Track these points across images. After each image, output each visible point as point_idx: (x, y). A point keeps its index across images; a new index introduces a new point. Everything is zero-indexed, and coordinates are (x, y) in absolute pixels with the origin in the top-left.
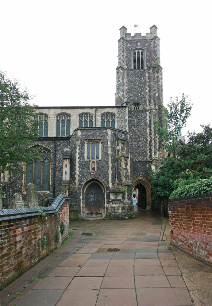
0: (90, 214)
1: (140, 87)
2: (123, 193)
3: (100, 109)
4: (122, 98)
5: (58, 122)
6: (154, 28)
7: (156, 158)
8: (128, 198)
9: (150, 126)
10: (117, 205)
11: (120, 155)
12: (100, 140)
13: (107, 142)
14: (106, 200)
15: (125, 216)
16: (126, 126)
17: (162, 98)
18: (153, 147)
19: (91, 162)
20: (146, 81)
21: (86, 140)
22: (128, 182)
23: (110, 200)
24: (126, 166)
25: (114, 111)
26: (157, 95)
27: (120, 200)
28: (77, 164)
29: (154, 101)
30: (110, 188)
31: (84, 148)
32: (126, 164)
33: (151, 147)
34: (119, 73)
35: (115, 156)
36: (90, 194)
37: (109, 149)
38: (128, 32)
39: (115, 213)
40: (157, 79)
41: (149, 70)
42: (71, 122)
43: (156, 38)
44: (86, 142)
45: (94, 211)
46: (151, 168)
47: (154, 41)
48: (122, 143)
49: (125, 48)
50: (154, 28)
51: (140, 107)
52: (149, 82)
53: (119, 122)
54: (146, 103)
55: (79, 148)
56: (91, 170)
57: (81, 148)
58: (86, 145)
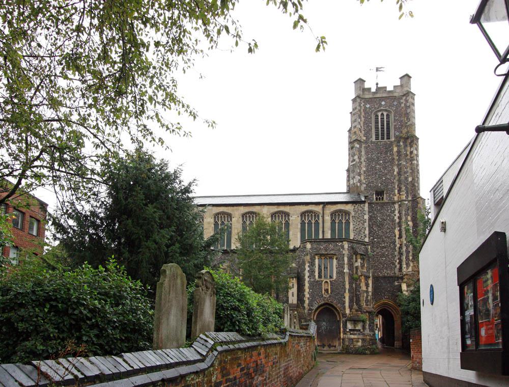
0: (321, 346)
1: (385, 168)
2: (364, 322)
3: (329, 206)
4: (359, 184)
6: (406, 78)
7: (409, 273)
8: (369, 328)
9: (400, 226)
10: (356, 337)
11: (360, 274)
12: (335, 255)
13: (343, 258)
14: (342, 329)
15: (366, 350)
16: (365, 228)
17: (418, 184)
18: (404, 258)
19: (323, 282)
20: (394, 159)
21: (316, 255)
22: (369, 308)
23: (348, 330)
24: (367, 288)
25: (349, 208)
26: (410, 179)
27: (360, 330)
28: (307, 285)
29: (407, 188)
30: (348, 315)
31: (315, 265)
32: (367, 285)
33: (401, 256)
34: (354, 149)
35: (353, 275)
36: (321, 321)
37: (346, 266)
38: (367, 86)
39: (354, 346)
40: (411, 155)
41: (399, 142)
42: (290, 223)
43: (409, 94)
44: (317, 257)
45: (326, 342)
46: (400, 286)
47: (406, 98)
48: (361, 259)
49: (362, 110)
50: (406, 78)
51: (385, 198)
52: (399, 160)
53: (355, 223)
54: (393, 190)
55: (308, 264)
56: (323, 293)
57: (311, 265)
58: (317, 261)
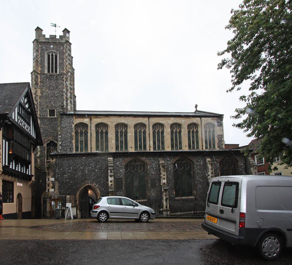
5: (117, 132)
50: (227, 27)
